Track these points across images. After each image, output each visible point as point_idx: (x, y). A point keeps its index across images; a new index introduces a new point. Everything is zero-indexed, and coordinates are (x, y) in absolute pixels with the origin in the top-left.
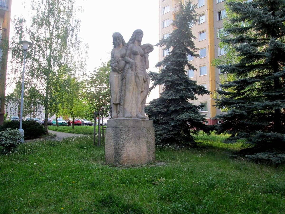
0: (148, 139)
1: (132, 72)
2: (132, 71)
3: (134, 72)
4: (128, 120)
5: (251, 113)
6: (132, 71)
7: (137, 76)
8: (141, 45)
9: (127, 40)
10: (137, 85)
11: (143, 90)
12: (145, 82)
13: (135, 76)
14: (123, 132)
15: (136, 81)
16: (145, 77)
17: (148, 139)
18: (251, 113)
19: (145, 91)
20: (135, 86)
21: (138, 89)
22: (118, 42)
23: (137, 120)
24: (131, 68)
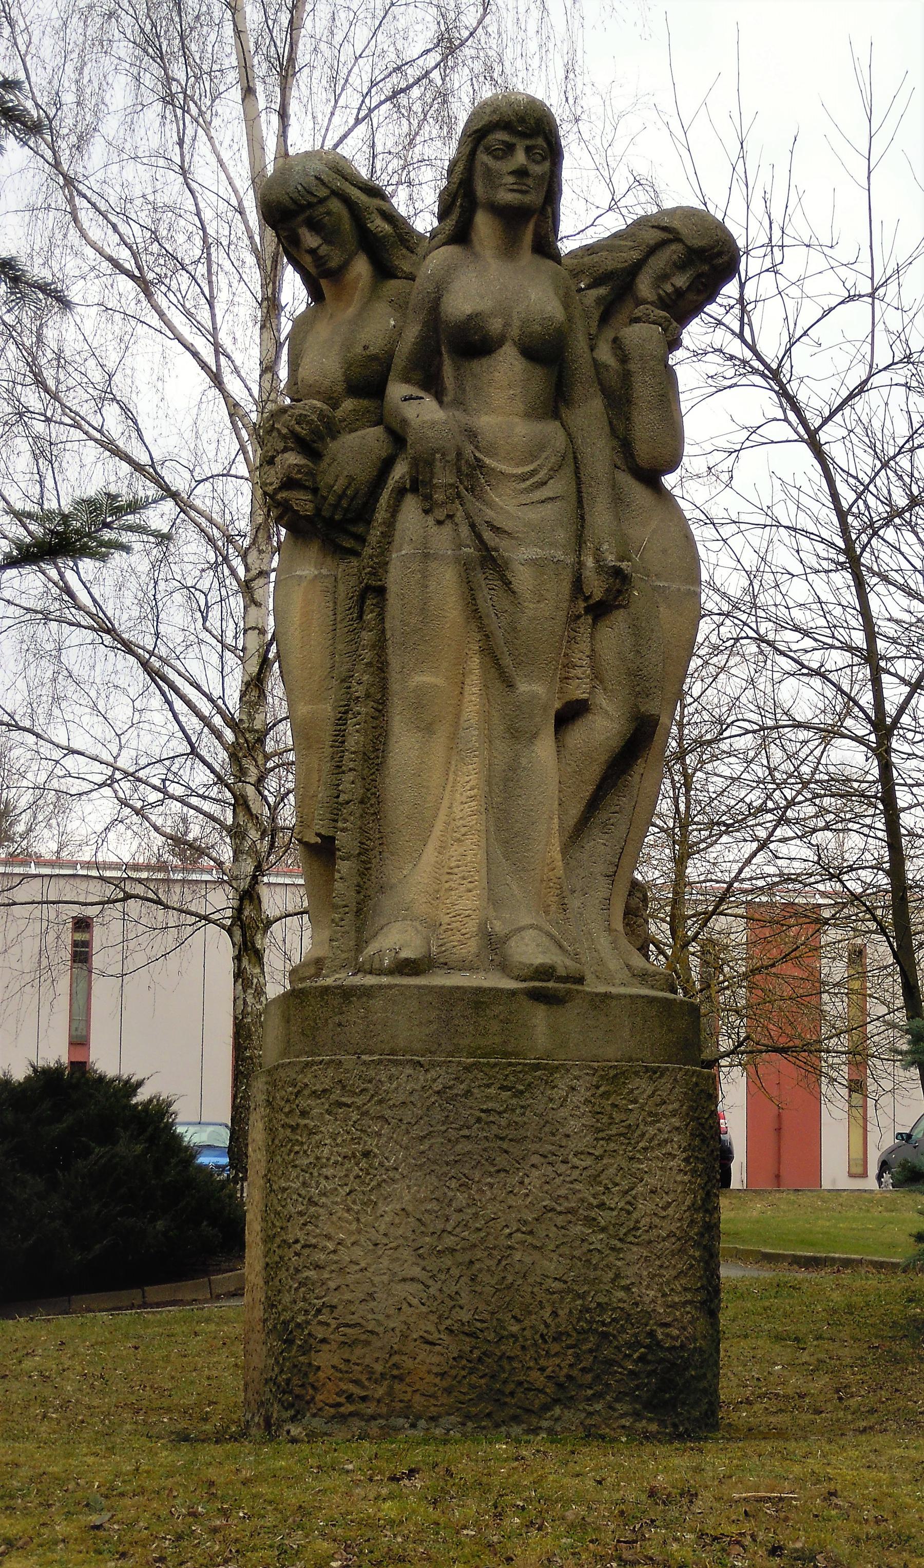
0: (595, 1179)
1: (435, 529)
2: (430, 520)
3: (447, 529)
4: (390, 987)
5: (237, 1174)
6: (430, 520)
7: (487, 563)
8: (566, 247)
9: (586, 216)
10: (490, 653)
11: (578, 691)
12: (600, 611)
13: (466, 567)
14: (317, 1108)
15: (474, 613)
16: (590, 562)
17: (595, 1179)
18: (237, 1174)
19: (602, 700)
20: (475, 663)
21: (510, 685)
22: (312, 252)
23: (480, 990)
24: (414, 489)
